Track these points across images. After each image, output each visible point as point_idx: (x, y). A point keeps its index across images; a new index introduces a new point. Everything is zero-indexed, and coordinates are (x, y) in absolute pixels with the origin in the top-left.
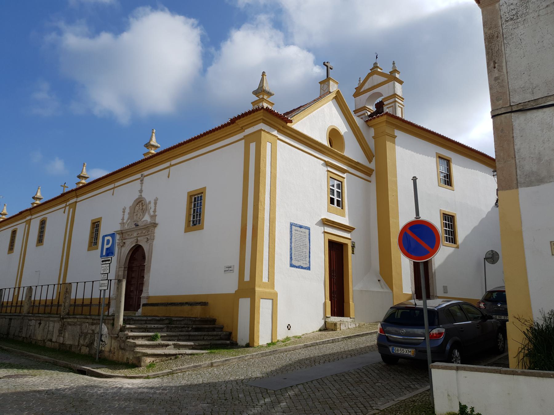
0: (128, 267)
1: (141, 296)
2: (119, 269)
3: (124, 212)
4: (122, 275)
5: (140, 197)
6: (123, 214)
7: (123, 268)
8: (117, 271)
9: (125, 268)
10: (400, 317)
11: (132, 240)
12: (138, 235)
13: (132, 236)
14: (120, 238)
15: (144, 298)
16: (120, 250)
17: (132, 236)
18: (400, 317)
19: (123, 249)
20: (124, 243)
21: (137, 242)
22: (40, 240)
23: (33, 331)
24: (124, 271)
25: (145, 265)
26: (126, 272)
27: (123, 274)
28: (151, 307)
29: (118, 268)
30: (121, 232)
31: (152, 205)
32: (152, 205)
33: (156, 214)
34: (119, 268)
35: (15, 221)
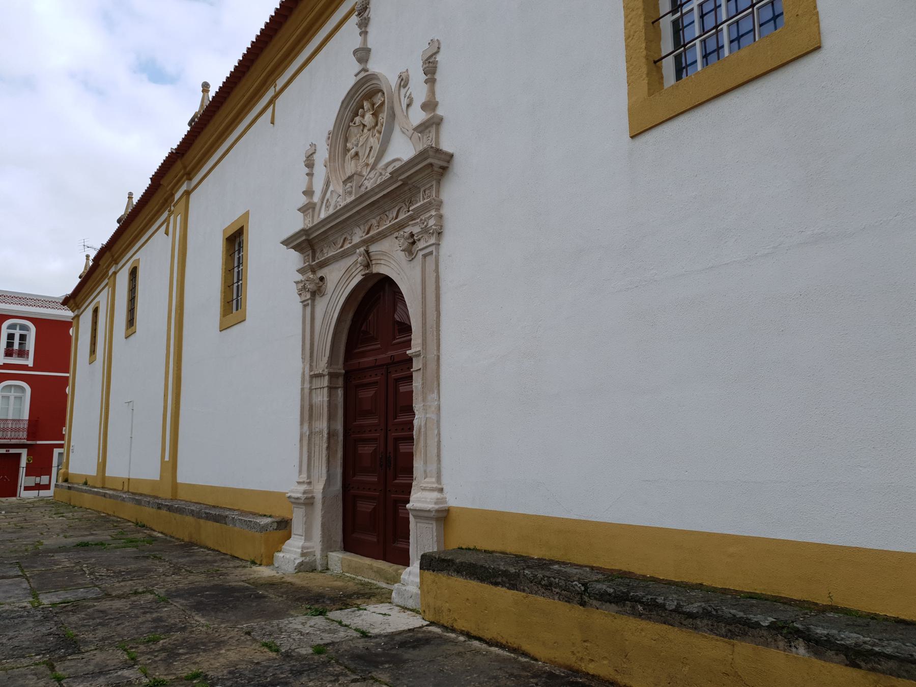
0: (343, 371)
1: (408, 506)
2: (311, 382)
3: (310, 163)
4: (326, 404)
5: (363, 74)
6: (307, 170)
7: (327, 378)
8: (307, 391)
9: (332, 376)
10: (168, 460)
11: (348, 262)
12: (371, 233)
13: (347, 246)
14: (305, 263)
15: (423, 515)
16: (309, 309)
17: (347, 246)
18: (168, 460)
19: (321, 305)
20: (322, 279)
21: (368, 266)
22: (324, 356)
23: (563, 670)
24: (332, 388)
25: (410, 360)
26: (340, 392)
27: (329, 402)
28: (474, 584)
29: (307, 377)
30: (304, 238)
31: (418, 90)
32: (418, 90)
33: (440, 111)
34: (312, 377)
35: (95, 285)
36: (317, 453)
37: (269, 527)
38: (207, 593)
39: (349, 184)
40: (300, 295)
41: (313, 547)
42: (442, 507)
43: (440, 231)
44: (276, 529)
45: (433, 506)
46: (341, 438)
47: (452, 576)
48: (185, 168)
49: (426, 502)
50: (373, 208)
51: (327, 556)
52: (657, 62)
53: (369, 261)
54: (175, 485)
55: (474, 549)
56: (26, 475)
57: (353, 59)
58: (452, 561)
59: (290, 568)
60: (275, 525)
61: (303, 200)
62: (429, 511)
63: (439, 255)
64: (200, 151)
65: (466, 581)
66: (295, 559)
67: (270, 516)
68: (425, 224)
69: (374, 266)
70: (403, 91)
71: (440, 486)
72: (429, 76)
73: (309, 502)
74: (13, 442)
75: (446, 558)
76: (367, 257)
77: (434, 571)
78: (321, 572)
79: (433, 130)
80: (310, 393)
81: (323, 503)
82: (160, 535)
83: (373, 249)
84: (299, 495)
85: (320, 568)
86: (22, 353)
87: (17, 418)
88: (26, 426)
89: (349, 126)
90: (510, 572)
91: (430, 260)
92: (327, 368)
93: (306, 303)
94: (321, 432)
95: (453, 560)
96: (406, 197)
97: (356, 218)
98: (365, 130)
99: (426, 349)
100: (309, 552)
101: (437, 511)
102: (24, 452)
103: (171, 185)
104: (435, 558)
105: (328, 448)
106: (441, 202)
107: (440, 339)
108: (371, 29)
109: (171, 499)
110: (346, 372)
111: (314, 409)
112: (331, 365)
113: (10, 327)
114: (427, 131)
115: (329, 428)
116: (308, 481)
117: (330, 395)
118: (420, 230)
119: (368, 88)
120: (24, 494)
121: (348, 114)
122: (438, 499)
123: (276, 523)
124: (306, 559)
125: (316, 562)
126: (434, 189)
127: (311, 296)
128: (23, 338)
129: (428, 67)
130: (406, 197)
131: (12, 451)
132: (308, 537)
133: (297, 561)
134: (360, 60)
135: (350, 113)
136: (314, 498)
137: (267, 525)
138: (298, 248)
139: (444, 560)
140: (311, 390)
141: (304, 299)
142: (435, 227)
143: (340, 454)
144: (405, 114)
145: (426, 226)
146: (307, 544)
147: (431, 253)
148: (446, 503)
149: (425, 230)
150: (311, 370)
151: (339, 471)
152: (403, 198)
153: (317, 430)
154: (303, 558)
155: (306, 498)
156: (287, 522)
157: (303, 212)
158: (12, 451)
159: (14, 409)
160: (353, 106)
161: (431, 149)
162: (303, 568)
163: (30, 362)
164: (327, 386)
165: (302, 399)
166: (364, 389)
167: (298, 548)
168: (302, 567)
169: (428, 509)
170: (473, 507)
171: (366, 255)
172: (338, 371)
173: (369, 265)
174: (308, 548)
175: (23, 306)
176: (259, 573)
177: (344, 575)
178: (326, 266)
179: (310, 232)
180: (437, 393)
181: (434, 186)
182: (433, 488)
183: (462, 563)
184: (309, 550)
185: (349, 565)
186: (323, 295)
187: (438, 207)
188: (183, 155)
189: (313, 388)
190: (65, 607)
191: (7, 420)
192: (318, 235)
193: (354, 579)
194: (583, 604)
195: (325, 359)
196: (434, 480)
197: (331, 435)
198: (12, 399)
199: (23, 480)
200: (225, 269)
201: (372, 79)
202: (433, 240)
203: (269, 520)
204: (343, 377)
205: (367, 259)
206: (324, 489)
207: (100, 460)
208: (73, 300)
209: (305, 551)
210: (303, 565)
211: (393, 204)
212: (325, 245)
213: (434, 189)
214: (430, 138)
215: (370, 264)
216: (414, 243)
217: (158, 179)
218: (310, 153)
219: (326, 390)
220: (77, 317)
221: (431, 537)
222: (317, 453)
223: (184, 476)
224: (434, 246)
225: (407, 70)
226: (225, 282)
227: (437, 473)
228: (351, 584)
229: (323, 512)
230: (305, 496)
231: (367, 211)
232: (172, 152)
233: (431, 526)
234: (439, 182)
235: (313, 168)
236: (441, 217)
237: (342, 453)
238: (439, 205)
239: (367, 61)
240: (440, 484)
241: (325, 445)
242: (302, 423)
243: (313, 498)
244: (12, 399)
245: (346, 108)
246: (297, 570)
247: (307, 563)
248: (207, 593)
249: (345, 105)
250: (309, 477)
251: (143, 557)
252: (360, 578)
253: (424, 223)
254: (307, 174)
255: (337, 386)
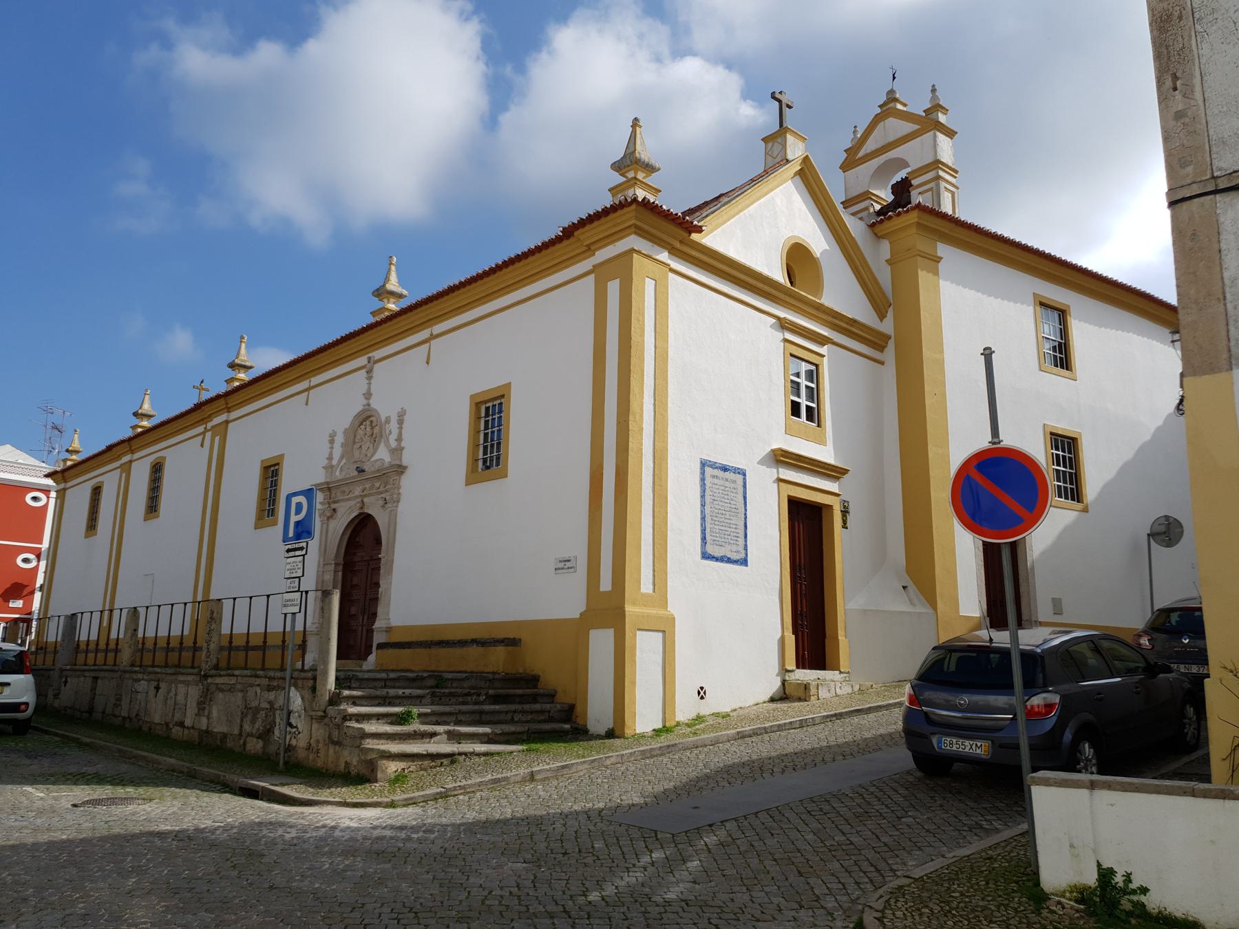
1: (373, 627)
2: (323, 568)
3: (332, 442)
4: (332, 580)
5: (367, 407)
7: (333, 566)
8: (320, 573)
9: (336, 564)
11: (352, 503)
16: (325, 526)
19: (333, 524)
20: (334, 510)
21: (362, 508)
24: (336, 571)
25: (380, 559)
26: (340, 573)
27: (334, 579)
29: (322, 566)
31: (394, 425)
32: (394, 425)
33: (403, 444)
34: (324, 565)
52: (477, 460)
61: (325, 462)
64: (1054, 275)
84: (313, 629)
101: (386, 628)
103: (866, 278)
108: (373, 381)
121: (357, 423)
133: (311, 664)
194: (430, 648)
216: (386, 503)
219: (332, 572)
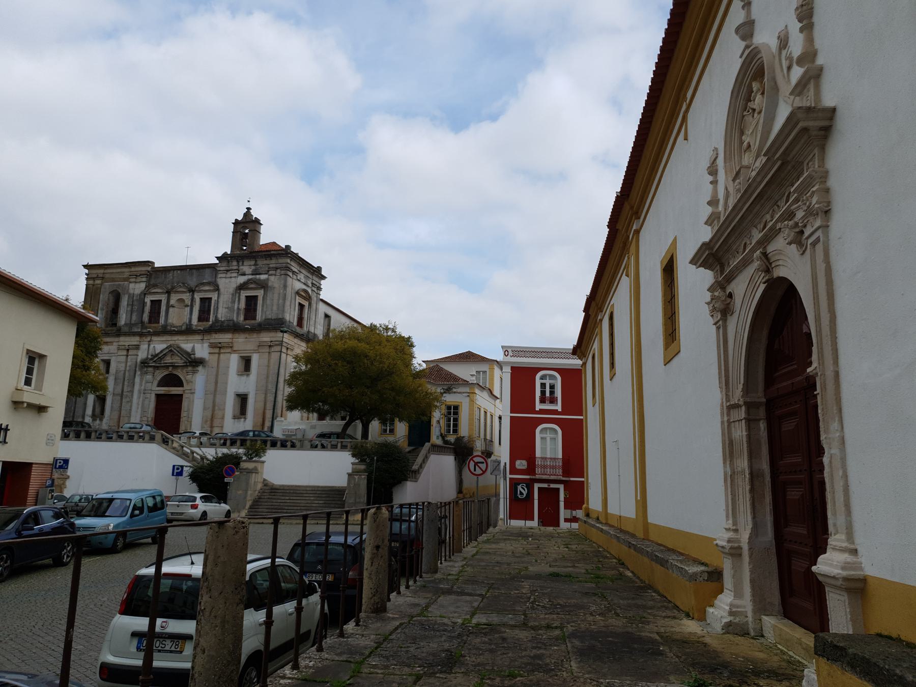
0: (764, 400)
2: (728, 415)
4: (745, 439)
6: (711, 178)
7: (743, 408)
9: (749, 406)
21: (768, 271)
24: (750, 422)
26: (763, 425)
27: (749, 437)
33: (820, 61)
36: (741, 497)
37: (699, 577)
38: (610, 639)
39: (738, 181)
40: (712, 316)
41: (745, 607)
42: (853, 575)
43: (827, 209)
44: (707, 581)
45: (840, 572)
46: (768, 478)
47: (846, 671)
48: (632, 208)
49: (831, 565)
50: (762, 201)
51: (760, 620)
53: (767, 264)
54: (646, 525)
55: (897, 639)
56: (565, 509)
57: (737, 38)
58: (843, 649)
59: (718, 627)
60: (706, 576)
61: (709, 210)
62: (834, 577)
63: (829, 240)
65: (860, 681)
66: (721, 617)
67: (702, 564)
68: (808, 204)
69: (774, 269)
70: (784, 53)
71: (852, 547)
72: (805, 22)
73: (735, 553)
74: (552, 477)
75: (838, 644)
76: (765, 261)
77: (828, 660)
78: (753, 638)
79: (811, 86)
80: (729, 426)
81: (750, 557)
82: (630, 574)
83: (770, 249)
84: (724, 544)
85: (752, 634)
86: (553, 400)
87: (553, 456)
88: (561, 464)
89: (743, 116)
90: (906, 680)
91: (819, 247)
92: (742, 397)
93: (718, 325)
94: (743, 472)
95: (845, 649)
96: (793, 177)
97: (749, 218)
98: (756, 115)
99: (823, 363)
100: (739, 612)
101: (846, 579)
102: (561, 487)
104: (828, 642)
105: (752, 490)
106: (827, 172)
107: (837, 349)
109: (643, 539)
110: (767, 400)
111: (734, 443)
112: (747, 394)
113: (542, 378)
114: (805, 90)
115: (751, 467)
116: (734, 528)
117: (749, 429)
118: (804, 213)
119: (755, 67)
120: (564, 525)
122: (849, 563)
123: (706, 574)
124: (735, 619)
125: (748, 624)
126: (817, 158)
127: (722, 316)
128: (552, 387)
129: (800, 12)
130: (793, 177)
131: (553, 486)
132: (738, 594)
133: (725, 620)
134: (743, 38)
135: (742, 101)
136: (741, 548)
137: (695, 574)
138: (705, 264)
139: (836, 647)
140: (729, 423)
141: (716, 320)
142: (818, 206)
143: (768, 498)
144: (787, 80)
145: (809, 207)
146: (738, 602)
147: (818, 240)
148: (861, 569)
149: (811, 213)
150: (728, 400)
151: (769, 520)
152: (791, 180)
153: (739, 469)
154: (732, 618)
155: (731, 548)
156: (719, 573)
157: (710, 225)
158: (553, 486)
159: (550, 448)
160: (745, 91)
161: (800, 110)
162: (729, 628)
163: (559, 407)
164: (745, 418)
165: (723, 434)
166: (792, 420)
167: (727, 605)
168: (731, 628)
169: (832, 575)
170: (892, 580)
171: (763, 258)
172: (757, 400)
173: (769, 269)
174: (738, 607)
175: (550, 359)
176: (683, 627)
177: (776, 646)
178: (733, 279)
179: (712, 244)
180: (838, 420)
181: (816, 155)
182: (842, 547)
183: (855, 654)
184: (739, 610)
185: (780, 635)
186: (732, 313)
187: (823, 180)
188: (628, 195)
189: (731, 421)
190: (485, 628)
191: (546, 458)
192: (719, 247)
193: (784, 653)
195: (741, 387)
196: (843, 537)
197: (754, 476)
198: (548, 439)
199: (563, 513)
200: (664, 300)
201: (756, 55)
202: (818, 223)
203: (703, 568)
204: (764, 407)
205: (764, 262)
206: (749, 538)
207: (639, 498)
208: (580, 349)
209: (734, 610)
210: (731, 626)
211: (782, 191)
212: (730, 256)
213: (817, 158)
214: (809, 98)
215: (770, 268)
217: (613, 223)
218: (713, 159)
219: (744, 421)
220: (584, 364)
221: (844, 613)
222: (741, 497)
223: (656, 516)
224: (820, 231)
225: (786, 26)
226: (665, 315)
227: (847, 529)
228: (776, 658)
229: (751, 566)
230: (730, 545)
231: (758, 207)
232: (617, 195)
233: (843, 599)
234: (823, 148)
235: (716, 174)
236: (827, 191)
237: (771, 497)
238: (825, 176)
239: (751, 35)
240: (853, 543)
241: (748, 488)
242: (725, 463)
243: (740, 548)
244: (548, 439)
245: (737, 96)
246: (724, 631)
247: (736, 624)
248: (610, 639)
249: (735, 94)
250: (735, 523)
251: (593, 593)
252: (791, 653)
253: (806, 204)
254: (711, 183)
255: (758, 418)
